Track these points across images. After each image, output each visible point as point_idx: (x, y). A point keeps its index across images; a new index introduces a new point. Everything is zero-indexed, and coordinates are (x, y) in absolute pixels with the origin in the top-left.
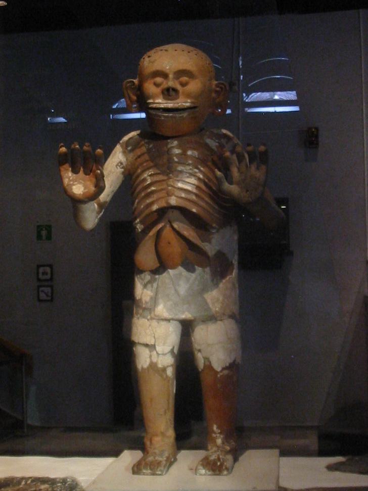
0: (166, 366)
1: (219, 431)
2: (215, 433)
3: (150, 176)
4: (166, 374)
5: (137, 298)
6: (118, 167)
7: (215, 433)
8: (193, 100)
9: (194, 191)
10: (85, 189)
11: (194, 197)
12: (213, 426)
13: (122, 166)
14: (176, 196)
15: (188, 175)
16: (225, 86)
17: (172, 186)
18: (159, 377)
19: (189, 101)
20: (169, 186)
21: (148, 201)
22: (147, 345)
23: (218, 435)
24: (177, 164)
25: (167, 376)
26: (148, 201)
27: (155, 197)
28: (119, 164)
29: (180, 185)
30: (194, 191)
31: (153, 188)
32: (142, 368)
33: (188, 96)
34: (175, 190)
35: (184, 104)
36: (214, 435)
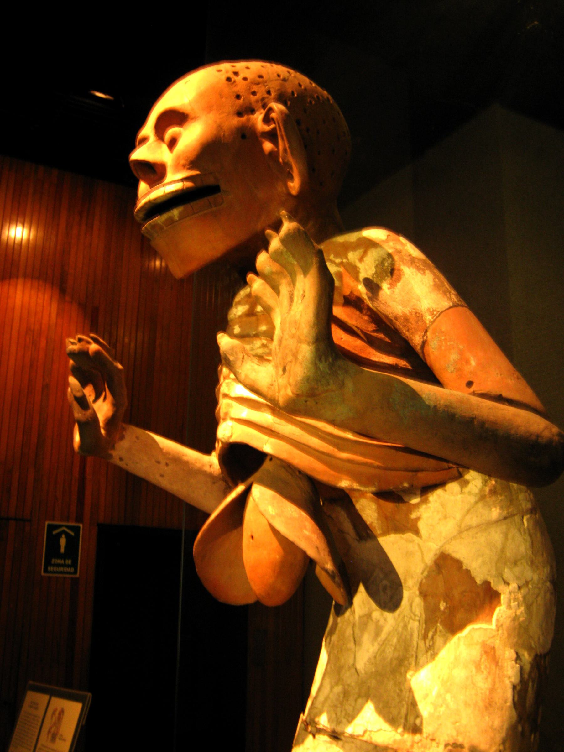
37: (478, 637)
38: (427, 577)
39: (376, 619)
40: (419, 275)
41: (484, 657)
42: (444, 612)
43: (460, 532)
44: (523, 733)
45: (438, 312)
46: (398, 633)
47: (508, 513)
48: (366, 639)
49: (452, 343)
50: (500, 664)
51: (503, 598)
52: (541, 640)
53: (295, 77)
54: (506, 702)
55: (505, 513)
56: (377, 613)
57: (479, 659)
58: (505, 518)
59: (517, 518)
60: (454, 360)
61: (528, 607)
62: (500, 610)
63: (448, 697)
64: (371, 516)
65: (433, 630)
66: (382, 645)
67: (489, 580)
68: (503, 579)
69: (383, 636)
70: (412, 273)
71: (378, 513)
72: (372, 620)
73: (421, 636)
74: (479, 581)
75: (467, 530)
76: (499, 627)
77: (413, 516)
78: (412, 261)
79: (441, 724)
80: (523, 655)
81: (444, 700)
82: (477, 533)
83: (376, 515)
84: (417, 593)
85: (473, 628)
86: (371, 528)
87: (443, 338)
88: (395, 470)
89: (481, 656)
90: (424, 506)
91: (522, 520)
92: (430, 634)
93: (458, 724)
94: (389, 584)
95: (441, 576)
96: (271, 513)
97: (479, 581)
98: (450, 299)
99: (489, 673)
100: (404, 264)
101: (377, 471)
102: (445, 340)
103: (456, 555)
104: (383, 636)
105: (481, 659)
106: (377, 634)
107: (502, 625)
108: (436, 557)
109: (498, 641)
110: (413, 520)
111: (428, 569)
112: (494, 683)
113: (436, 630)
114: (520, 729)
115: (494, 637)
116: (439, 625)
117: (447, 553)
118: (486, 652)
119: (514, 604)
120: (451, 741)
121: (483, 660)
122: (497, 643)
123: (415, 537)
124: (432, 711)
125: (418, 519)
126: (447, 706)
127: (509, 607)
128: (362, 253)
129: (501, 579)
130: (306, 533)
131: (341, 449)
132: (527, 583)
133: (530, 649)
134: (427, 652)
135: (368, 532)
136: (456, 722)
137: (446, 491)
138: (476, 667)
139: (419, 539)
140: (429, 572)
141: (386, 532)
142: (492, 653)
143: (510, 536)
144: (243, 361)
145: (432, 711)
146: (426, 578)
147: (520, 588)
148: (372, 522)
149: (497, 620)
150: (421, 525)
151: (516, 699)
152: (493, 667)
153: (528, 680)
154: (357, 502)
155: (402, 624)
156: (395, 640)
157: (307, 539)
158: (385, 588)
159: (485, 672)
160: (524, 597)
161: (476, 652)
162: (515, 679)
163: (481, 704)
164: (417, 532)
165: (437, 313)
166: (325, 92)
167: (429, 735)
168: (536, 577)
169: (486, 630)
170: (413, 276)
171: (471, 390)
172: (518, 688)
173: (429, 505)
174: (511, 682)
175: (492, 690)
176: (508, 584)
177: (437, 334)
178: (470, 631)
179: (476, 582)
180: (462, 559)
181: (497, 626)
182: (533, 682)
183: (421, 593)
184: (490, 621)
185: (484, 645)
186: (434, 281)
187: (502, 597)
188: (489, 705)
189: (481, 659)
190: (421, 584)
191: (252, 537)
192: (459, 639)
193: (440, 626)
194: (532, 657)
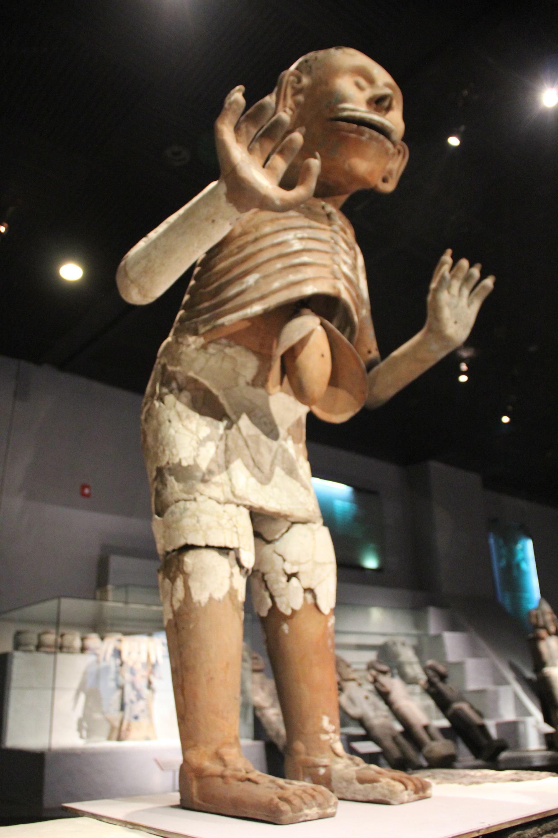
2: (327, 732)
3: (301, 239)
5: (184, 464)
7: (327, 732)
12: (320, 719)
16: (404, 150)
20: (334, 261)
21: (292, 277)
22: (224, 550)
23: (332, 735)
26: (292, 277)
27: (309, 272)
31: (305, 258)
32: (211, 598)
36: (324, 737)
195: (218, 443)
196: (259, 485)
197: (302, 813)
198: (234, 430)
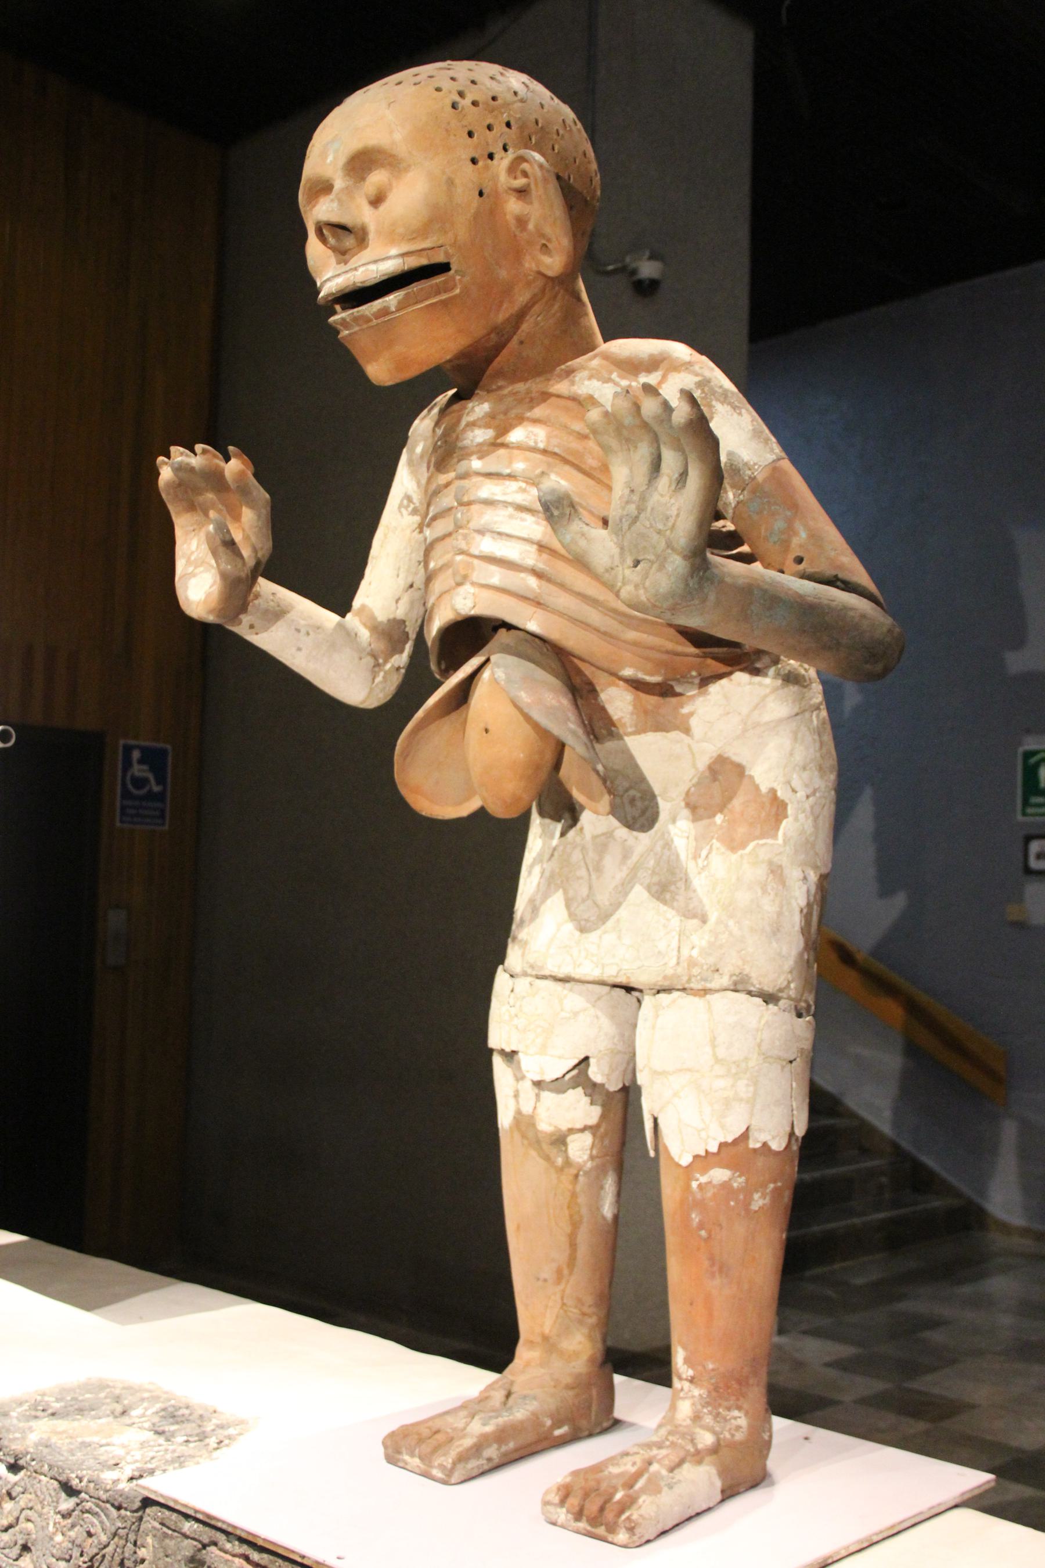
0: (564, 1127)
1: (691, 1373)
4: (566, 1151)
6: (403, 510)
8: (405, 248)
9: (530, 557)
10: (805, 693)
11: (532, 582)
13: (412, 506)
14: (473, 584)
15: (510, 510)
17: (462, 552)
18: (542, 1162)
19: (394, 251)
24: (480, 479)
25: (568, 1162)
28: (405, 502)
29: (487, 545)
30: (530, 557)
33: (391, 236)
34: (476, 562)
35: (373, 267)
37: (764, 854)
38: (698, 785)
39: (621, 838)
40: (735, 415)
41: (771, 877)
42: (721, 827)
43: (745, 731)
44: (808, 960)
45: (760, 466)
46: (656, 854)
47: (800, 708)
48: (609, 862)
49: (778, 508)
50: (787, 884)
51: (790, 810)
52: (825, 858)
53: (558, 104)
54: (794, 927)
55: (796, 710)
56: (622, 832)
57: (765, 879)
58: (797, 714)
59: (807, 715)
60: (779, 529)
61: (816, 819)
62: (787, 822)
63: (731, 923)
64: (622, 709)
65: (708, 847)
66: (632, 869)
67: (775, 788)
68: (791, 787)
69: (634, 858)
70: (727, 411)
71: (635, 706)
72: (615, 840)
73: (690, 856)
74: (764, 789)
75: (754, 728)
76: (785, 842)
77: (685, 710)
78: (725, 397)
79: (724, 954)
80: (809, 874)
81: (726, 926)
82: (764, 732)
83: (630, 708)
84: (683, 804)
85: (758, 844)
86: (618, 725)
87: (766, 500)
88: (683, 656)
89: (768, 875)
90: (701, 699)
91: (811, 716)
92: (704, 853)
93: (743, 952)
94: (638, 795)
95: (717, 783)
96: (526, 700)
97: (764, 789)
98: (772, 450)
99: (776, 895)
100: (717, 400)
101: (665, 657)
102: (769, 502)
103: (736, 759)
104: (634, 858)
105: (767, 879)
106: (626, 856)
107: (789, 840)
108: (711, 761)
109: (785, 858)
110: (683, 715)
111: (699, 775)
112: (781, 906)
113: (711, 846)
114: (806, 957)
115: (780, 853)
116: (714, 841)
117: (726, 755)
118: (772, 872)
119: (801, 816)
120: (737, 972)
121: (769, 880)
122: (784, 861)
123: (683, 736)
124: (713, 939)
125: (691, 714)
126: (731, 934)
127: (796, 819)
128: (660, 378)
129: (789, 788)
130: (572, 726)
131: (629, 626)
132: (814, 793)
133: (815, 867)
134: (699, 873)
135: (613, 729)
136: (741, 951)
137: (731, 680)
138: (762, 888)
139: (689, 738)
140: (699, 779)
141: (640, 731)
142: (779, 872)
143: (800, 735)
144: (569, 519)
145: (713, 939)
146: (694, 785)
147: (808, 797)
148: (622, 717)
149: (784, 834)
150: (693, 722)
151: (803, 924)
152: (780, 887)
153: (813, 902)
154: (602, 690)
155: (661, 843)
156: (652, 863)
157: (574, 733)
158: (632, 801)
159: (772, 893)
160: (812, 807)
161: (761, 872)
162: (802, 902)
163: (768, 929)
164: (687, 731)
165: (758, 468)
166: (516, 80)
167: (710, 966)
168: (823, 786)
169: (772, 845)
170: (729, 417)
171: (801, 567)
172: (805, 911)
173: (709, 697)
174: (798, 904)
175: (780, 914)
176: (796, 792)
177: (758, 494)
178: (754, 849)
179: (760, 791)
180: (744, 763)
181: (784, 840)
182: (817, 904)
183: (688, 805)
184: (775, 836)
185: (770, 863)
186: (753, 425)
187: (789, 807)
188: (776, 930)
189: (767, 879)
190: (687, 793)
191: (487, 731)
192: (742, 856)
193: (716, 844)
194: (818, 876)
195: (545, 866)
196: (577, 933)
197: (401, 1457)
198: (572, 833)
